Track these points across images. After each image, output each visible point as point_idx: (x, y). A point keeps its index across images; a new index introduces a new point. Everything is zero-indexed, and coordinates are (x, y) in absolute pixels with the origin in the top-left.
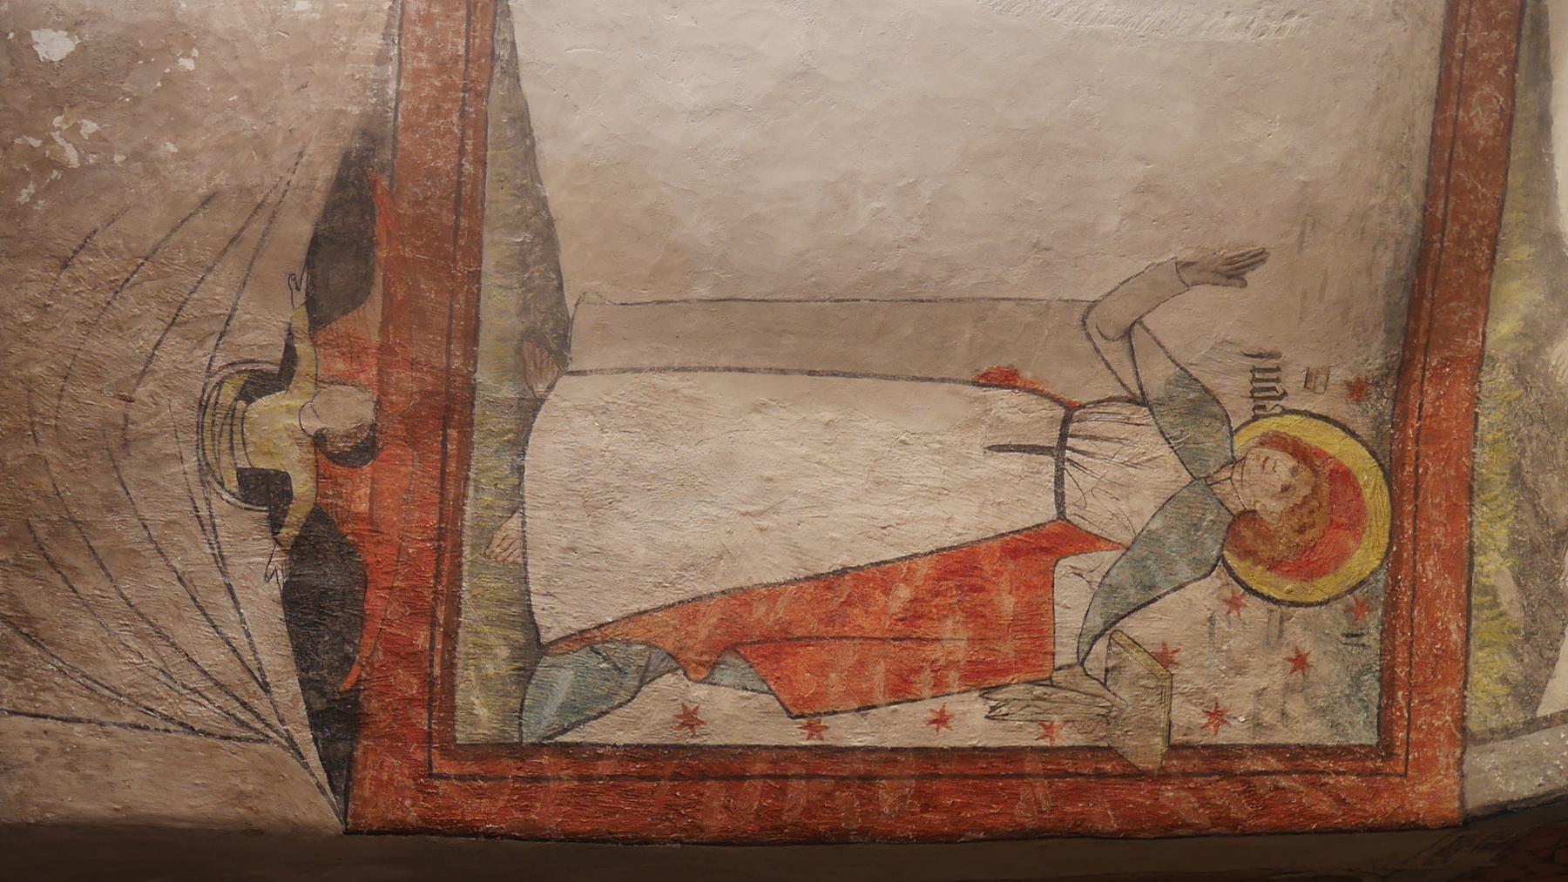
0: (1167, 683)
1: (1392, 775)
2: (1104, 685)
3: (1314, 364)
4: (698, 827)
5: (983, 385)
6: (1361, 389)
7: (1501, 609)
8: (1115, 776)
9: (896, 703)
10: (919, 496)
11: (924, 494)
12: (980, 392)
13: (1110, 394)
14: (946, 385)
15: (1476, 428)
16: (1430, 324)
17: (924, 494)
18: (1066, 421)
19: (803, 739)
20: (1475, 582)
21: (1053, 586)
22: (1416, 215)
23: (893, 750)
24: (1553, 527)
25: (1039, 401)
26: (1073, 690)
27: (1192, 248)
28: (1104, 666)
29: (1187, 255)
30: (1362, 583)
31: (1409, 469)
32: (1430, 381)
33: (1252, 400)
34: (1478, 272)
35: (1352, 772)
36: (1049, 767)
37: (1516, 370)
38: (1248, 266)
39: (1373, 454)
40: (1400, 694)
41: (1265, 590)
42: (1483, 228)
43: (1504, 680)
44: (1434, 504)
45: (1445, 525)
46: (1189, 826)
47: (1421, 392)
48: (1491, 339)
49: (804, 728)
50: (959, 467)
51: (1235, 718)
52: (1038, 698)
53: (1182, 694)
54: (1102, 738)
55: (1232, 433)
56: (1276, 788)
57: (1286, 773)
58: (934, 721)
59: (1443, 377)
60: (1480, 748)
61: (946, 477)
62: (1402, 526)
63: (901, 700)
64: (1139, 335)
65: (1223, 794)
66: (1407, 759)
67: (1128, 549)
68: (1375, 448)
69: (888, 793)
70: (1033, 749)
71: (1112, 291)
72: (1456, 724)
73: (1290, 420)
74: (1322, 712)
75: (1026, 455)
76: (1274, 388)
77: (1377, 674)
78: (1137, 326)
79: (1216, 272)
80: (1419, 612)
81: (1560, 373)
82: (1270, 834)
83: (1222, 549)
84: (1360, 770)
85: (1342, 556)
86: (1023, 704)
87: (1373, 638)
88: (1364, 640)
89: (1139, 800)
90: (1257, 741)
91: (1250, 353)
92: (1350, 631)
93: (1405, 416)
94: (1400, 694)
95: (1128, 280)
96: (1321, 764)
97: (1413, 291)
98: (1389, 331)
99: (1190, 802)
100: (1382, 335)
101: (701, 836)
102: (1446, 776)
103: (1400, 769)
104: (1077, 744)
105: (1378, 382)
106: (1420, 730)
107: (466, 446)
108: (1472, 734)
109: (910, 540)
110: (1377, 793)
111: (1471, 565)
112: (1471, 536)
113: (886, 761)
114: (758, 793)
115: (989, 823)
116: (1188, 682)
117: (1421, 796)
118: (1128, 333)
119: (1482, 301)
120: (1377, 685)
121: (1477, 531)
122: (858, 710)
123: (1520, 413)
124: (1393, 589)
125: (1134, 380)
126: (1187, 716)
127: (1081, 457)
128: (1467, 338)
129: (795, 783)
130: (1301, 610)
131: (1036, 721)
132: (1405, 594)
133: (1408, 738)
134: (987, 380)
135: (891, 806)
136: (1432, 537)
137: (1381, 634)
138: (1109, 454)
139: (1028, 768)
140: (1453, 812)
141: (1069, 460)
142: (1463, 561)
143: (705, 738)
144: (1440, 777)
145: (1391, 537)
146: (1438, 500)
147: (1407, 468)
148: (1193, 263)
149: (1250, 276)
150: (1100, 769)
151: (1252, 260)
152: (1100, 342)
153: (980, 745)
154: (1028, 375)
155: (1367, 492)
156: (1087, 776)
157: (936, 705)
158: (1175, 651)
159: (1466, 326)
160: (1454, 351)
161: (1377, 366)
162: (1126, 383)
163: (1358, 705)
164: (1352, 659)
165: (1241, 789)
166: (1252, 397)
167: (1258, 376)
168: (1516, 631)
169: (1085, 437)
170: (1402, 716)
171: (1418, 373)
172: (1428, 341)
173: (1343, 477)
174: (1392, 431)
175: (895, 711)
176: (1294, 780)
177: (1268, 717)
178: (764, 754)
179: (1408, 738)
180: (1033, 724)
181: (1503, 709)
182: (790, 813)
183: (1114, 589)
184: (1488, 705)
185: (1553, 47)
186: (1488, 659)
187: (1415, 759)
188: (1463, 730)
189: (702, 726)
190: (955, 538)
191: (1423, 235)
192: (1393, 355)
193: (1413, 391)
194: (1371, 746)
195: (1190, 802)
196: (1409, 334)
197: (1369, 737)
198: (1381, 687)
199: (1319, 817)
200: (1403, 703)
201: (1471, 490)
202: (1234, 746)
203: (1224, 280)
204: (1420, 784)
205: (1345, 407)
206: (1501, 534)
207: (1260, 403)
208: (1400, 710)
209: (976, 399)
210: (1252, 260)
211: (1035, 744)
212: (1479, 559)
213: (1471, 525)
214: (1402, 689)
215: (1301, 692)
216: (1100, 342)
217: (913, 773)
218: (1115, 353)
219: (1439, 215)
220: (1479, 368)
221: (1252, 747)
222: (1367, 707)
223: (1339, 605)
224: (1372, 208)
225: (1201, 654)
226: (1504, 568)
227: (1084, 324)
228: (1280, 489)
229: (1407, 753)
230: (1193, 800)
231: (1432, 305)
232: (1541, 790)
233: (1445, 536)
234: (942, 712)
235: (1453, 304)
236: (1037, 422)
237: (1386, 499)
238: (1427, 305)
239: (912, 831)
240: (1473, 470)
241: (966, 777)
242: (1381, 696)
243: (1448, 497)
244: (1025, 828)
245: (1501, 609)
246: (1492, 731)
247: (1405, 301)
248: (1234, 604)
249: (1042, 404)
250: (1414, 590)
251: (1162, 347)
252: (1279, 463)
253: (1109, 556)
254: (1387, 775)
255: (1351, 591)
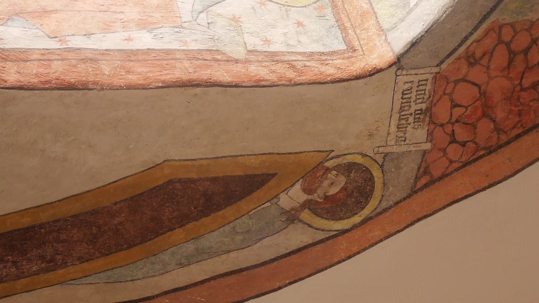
0: (239, 28)
1: (358, 56)
4: (3, 80)
9: (105, 33)
19: (58, 46)
28: (206, 22)
35: (339, 59)
49: (58, 42)
52: (177, 32)
56: (305, 66)
63: (107, 32)
65: (280, 69)
66: (363, 50)
82: (309, 84)
84: (342, 57)
88: (327, 18)
92: (319, 15)
94: (350, 31)
96: (324, 58)
101: (5, 84)
102: (382, 48)
103: (361, 53)
107: (41, 226)
113: (103, 54)
114: (35, 66)
116: (249, 28)
122: (85, 35)
129: (55, 62)
131: (177, 40)
133: (360, 43)
139: (178, 56)
140: (391, 57)
143: (4, 45)
144: (380, 49)
150: (215, 58)
157: (126, 34)
175: (104, 36)
176: (313, 63)
178: (37, 51)
179: (360, 43)
181: (396, 15)
182: (54, 74)
184: (389, 17)
187: (366, 49)
189: (2, 40)
198: (341, 31)
200: (353, 34)
204: (372, 55)
225: (252, 19)
232: (424, 26)
239: (123, 83)
242: (342, 34)
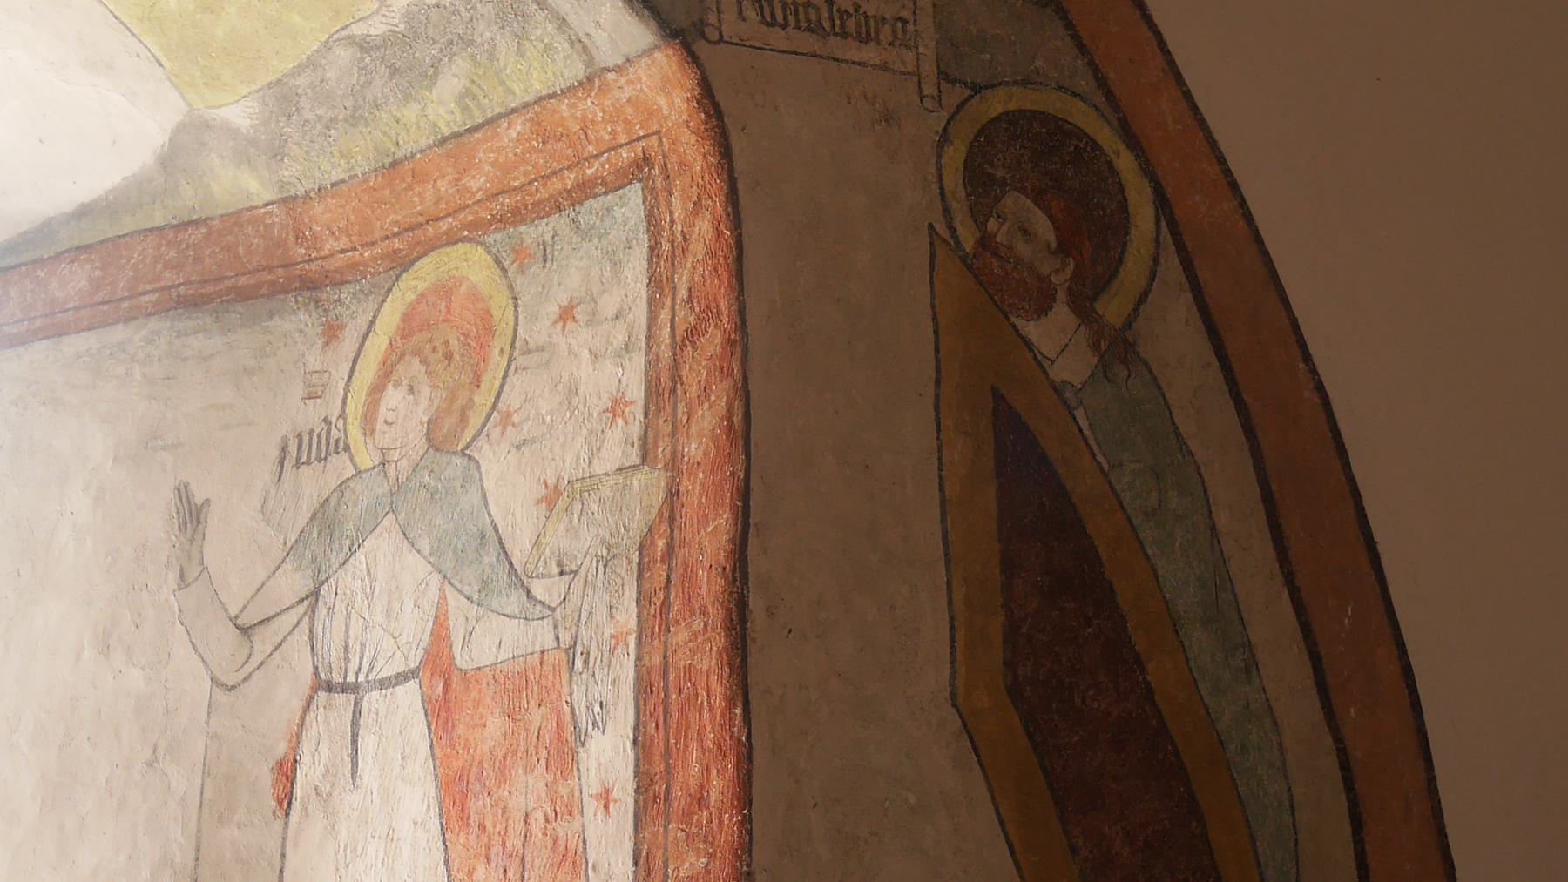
1: (663, 151)
2: (575, 573)
3: (299, 391)
5: (290, 803)
6: (330, 327)
7: (468, 85)
8: (672, 531)
10: (392, 868)
11: (391, 861)
12: (296, 804)
13: (305, 638)
14: (288, 851)
15: (343, 181)
16: (263, 270)
17: (391, 861)
18: (330, 687)
20: (466, 124)
21: (479, 669)
22: (154, 323)
23: (636, 863)
24: (362, 59)
25: (308, 726)
26: (580, 616)
27: (167, 574)
28: (557, 578)
29: (172, 577)
30: (498, 262)
31: (397, 243)
32: (321, 249)
33: (329, 458)
34: (208, 236)
35: (669, 204)
36: (657, 629)
37: (279, 158)
38: (189, 503)
39: (389, 290)
40: (589, 172)
41: (497, 383)
42: (169, 244)
43: (520, 53)
44: (422, 200)
45: (435, 181)
46: (730, 410)
47: (331, 255)
48: (268, 197)
50: (370, 820)
51: (620, 381)
52: (586, 662)
53: (590, 462)
54: (630, 562)
55: (359, 473)
56: (690, 300)
57: (674, 290)
58: (606, 806)
59: (315, 237)
60: (594, 52)
61: (377, 836)
62: (446, 233)
63: (584, 860)
64: (244, 620)
65: (696, 371)
66: (644, 137)
67: (445, 577)
68: (383, 292)
69: (683, 862)
70: (639, 658)
71: (203, 660)
72: (591, 90)
73: (350, 408)
74: (616, 265)
75: (361, 733)
76: (319, 435)
77: (577, 209)
78: (239, 622)
79: (191, 541)
80: (515, 179)
81: (252, 111)
83: (455, 453)
85: (475, 296)
86: (591, 681)
87: (543, 229)
88: (548, 237)
89: (698, 488)
90: (643, 345)
91: (277, 475)
93: (353, 266)
95: (192, 643)
96: (666, 247)
97: (228, 301)
98: (271, 316)
99: (703, 415)
100: (277, 321)
102: (640, 80)
103: (654, 140)
104: (635, 597)
105: (325, 310)
106: (614, 133)
108: (587, 67)
109: (432, 872)
110: (683, 164)
111: (456, 135)
112: (430, 147)
115: (719, 702)
116: (578, 458)
117: (671, 104)
118: (245, 631)
119: (235, 220)
120: (586, 204)
121: (424, 143)
123: (307, 137)
124: (500, 220)
125: (294, 611)
126: (617, 447)
127: (365, 660)
128: (273, 223)
130: (520, 330)
132: (502, 205)
133: (626, 144)
134: (285, 801)
135: (698, 856)
136: (450, 192)
137: (542, 218)
138: (361, 624)
139: (657, 660)
141: (367, 676)
142: (455, 144)
145: (456, 242)
146: (416, 199)
147: (397, 246)
148: (182, 570)
149: (198, 499)
151: (184, 500)
152: (255, 661)
153: (631, 736)
154: (282, 748)
155: (422, 286)
156: (670, 569)
157: (591, 806)
158: (546, 485)
159: (262, 228)
160: (287, 234)
161: (307, 317)
162: (296, 620)
163: (607, 222)
164: (566, 247)
165: (689, 348)
166: (326, 458)
167: (304, 459)
168: (473, 57)
169: (347, 659)
170: (608, 160)
171: (313, 266)
172: (281, 266)
173: (410, 324)
174: (369, 276)
176: (680, 279)
177: (619, 337)
179: (626, 144)
180: (613, 663)
181: (546, 41)
183: (485, 584)
184: (553, 61)
185: (25, 227)
186: (516, 79)
187: (642, 128)
188: (590, 79)
190: (432, 813)
191: (171, 309)
192: (297, 301)
193: (330, 265)
194: (643, 189)
195: (703, 415)
196: (278, 290)
197: (635, 193)
199: (716, 229)
200: (597, 164)
201: (394, 164)
202: (646, 374)
203: (201, 527)
205: (347, 341)
206: (410, 113)
207: (332, 448)
208: (603, 165)
209: (304, 809)
210: (184, 500)
211: (633, 657)
212: (447, 132)
213: (422, 151)
214: (584, 171)
215: (596, 302)
216: (255, 661)
217: (662, 829)
218: (263, 642)
219: (153, 297)
220: (295, 198)
221: (649, 347)
222: (608, 209)
223: (518, 282)
224: (144, 375)
226: (434, 96)
227: (233, 687)
228: (411, 397)
229: (639, 139)
230: (700, 413)
231: (244, 274)
233: (444, 176)
234: (598, 797)
235: (241, 250)
236: (329, 724)
237: (426, 260)
238: (243, 280)
239: (732, 816)
240: (376, 170)
241: (667, 749)
242: (596, 196)
243: (410, 188)
244: (725, 648)
245: (468, 85)
246: (572, 43)
247: (240, 308)
248: (506, 421)
249: (311, 722)
250: (498, 194)
251: (263, 584)
252: (389, 407)
253: (455, 602)
254: (664, 157)
255: (504, 270)
